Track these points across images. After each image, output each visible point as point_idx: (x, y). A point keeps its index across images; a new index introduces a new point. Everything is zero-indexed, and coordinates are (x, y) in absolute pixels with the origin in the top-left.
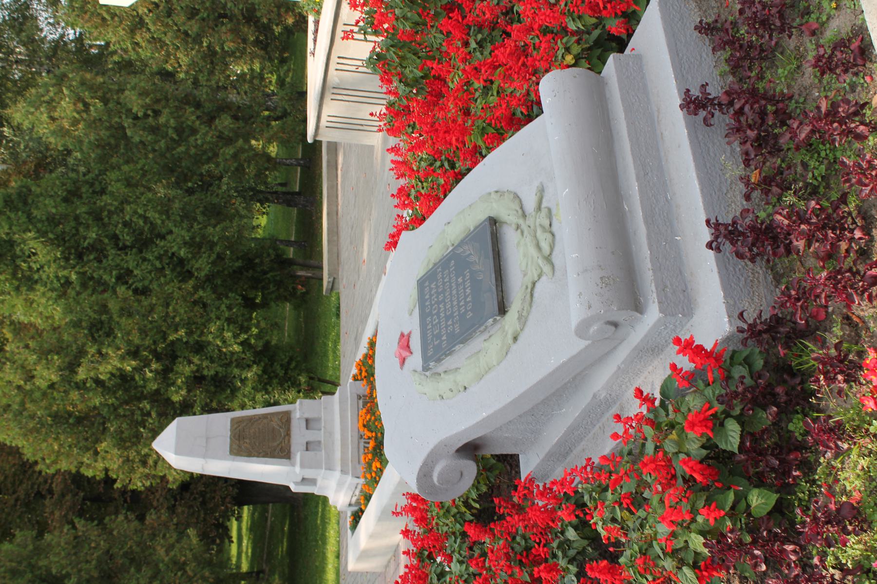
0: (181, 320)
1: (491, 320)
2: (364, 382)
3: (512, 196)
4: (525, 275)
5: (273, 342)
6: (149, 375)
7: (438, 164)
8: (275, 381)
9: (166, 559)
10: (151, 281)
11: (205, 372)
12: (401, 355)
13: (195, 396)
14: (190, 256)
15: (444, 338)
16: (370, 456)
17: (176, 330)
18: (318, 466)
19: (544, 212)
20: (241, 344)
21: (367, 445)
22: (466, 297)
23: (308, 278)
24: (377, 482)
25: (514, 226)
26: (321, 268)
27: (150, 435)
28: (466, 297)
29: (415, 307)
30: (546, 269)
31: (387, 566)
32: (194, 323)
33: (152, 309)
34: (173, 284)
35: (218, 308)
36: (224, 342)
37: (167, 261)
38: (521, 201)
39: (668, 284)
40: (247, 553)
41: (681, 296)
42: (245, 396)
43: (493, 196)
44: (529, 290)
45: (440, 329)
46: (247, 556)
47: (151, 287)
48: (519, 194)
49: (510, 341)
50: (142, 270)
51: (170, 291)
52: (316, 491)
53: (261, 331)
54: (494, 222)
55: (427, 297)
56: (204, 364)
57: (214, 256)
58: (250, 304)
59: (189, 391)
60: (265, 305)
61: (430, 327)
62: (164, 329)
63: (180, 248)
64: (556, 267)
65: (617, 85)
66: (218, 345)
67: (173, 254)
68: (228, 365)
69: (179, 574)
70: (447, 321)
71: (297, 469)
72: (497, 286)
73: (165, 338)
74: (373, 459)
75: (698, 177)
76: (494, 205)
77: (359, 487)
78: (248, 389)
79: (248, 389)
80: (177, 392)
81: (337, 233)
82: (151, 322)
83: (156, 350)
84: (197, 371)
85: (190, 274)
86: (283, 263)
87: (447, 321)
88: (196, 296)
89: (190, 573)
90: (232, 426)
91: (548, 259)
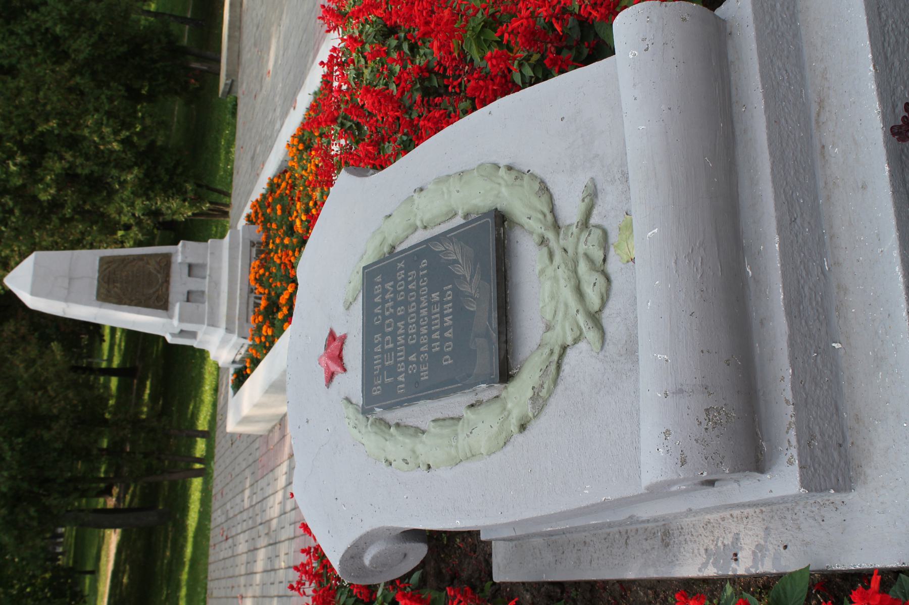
0: (53, 109)
1: (484, 386)
2: (260, 227)
3: (536, 186)
4: (549, 328)
5: (159, 143)
6: (13, 168)
7: (394, 43)
8: (158, 187)
9: (26, 376)
10: (19, 59)
11: (79, 171)
12: (328, 366)
13: (66, 196)
14: (67, 34)
15: (401, 378)
16: (260, 318)
17: (47, 121)
18: (200, 321)
19: (596, 234)
20: (122, 142)
21: (258, 301)
22: (443, 330)
23: (202, 71)
24: (268, 349)
25: (536, 239)
26: (218, 61)
27: (13, 233)
28: (443, 330)
29: (355, 299)
30: (591, 335)
31: (271, 431)
32: (68, 114)
33: (19, 92)
34: (44, 66)
35: (97, 99)
36: (102, 138)
37: (39, 38)
38: (551, 197)
39: (817, 430)
40: (120, 345)
41: (836, 455)
42: (123, 200)
43: (502, 172)
44: (555, 357)
45: (396, 362)
46: (120, 349)
47: (19, 66)
48: (549, 185)
49: (514, 428)
50: (9, 45)
51: (42, 74)
52: (196, 344)
53: (144, 128)
54: (501, 220)
55: (377, 300)
56: (78, 161)
57: (95, 38)
58: (134, 96)
59: (59, 190)
60: (151, 98)
61: (378, 349)
62: (32, 117)
63: (55, 25)
64: (609, 336)
65: (754, 46)
66: (94, 142)
67: (47, 30)
68: (105, 164)
69: (40, 393)
70: (408, 354)
71: (175, 322)
72: (499, 333)
73: (33, 127)
74: (264, 322)
75: (902, 260)
76: (504, 190)
77: (246, 347)
78: (127, 194)
79: (127, 194)
80: (45, 190)
81: (240, 28)
82: (17, 107)
83: (21, 141)
84: (70, 168)
85: (66, 55)
86: (175, 51)
87: (408, 354)
88: (72, 83)
89: (52, 393)
90: (101, 266)
91: (595, 318)
